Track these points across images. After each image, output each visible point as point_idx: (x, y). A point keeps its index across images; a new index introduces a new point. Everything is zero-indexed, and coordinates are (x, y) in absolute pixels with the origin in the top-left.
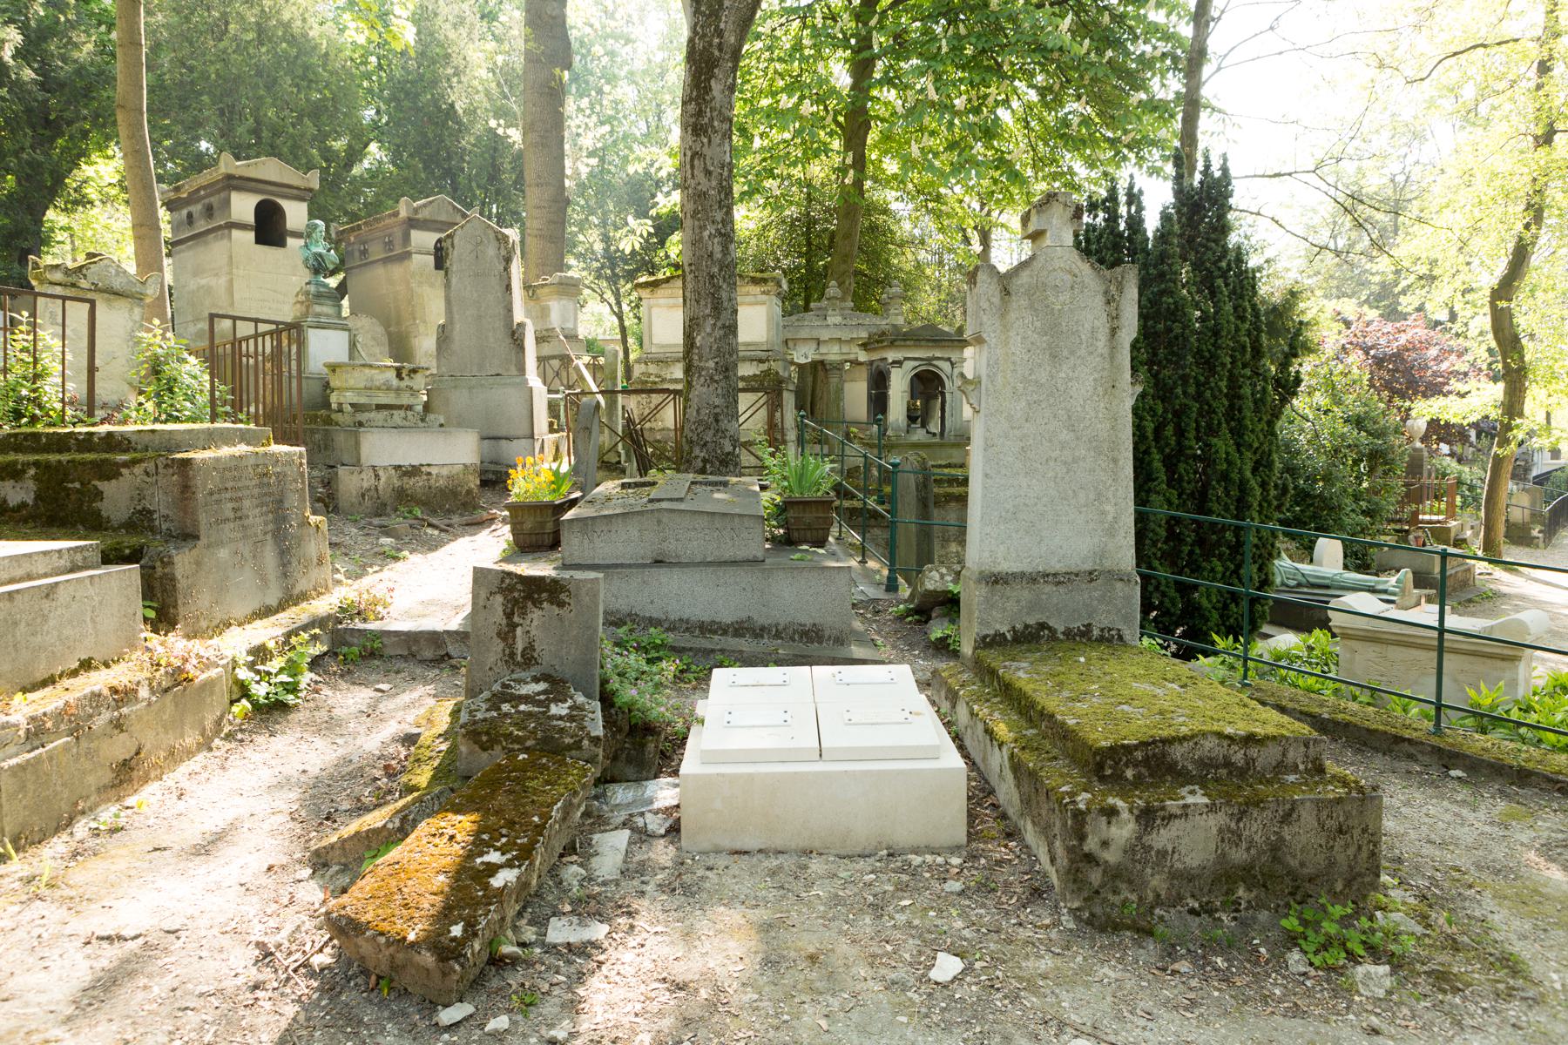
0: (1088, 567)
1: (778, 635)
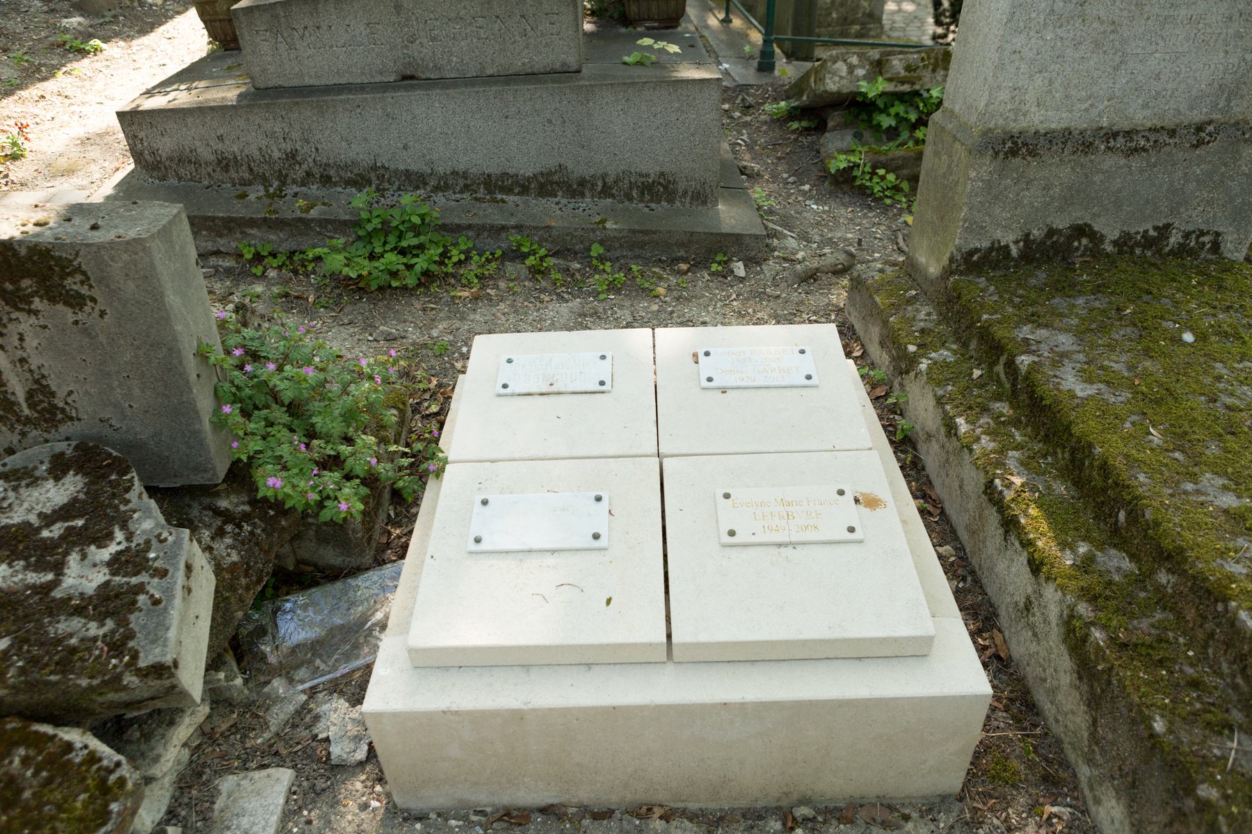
0: (1197, 116)
1: (606, 192)
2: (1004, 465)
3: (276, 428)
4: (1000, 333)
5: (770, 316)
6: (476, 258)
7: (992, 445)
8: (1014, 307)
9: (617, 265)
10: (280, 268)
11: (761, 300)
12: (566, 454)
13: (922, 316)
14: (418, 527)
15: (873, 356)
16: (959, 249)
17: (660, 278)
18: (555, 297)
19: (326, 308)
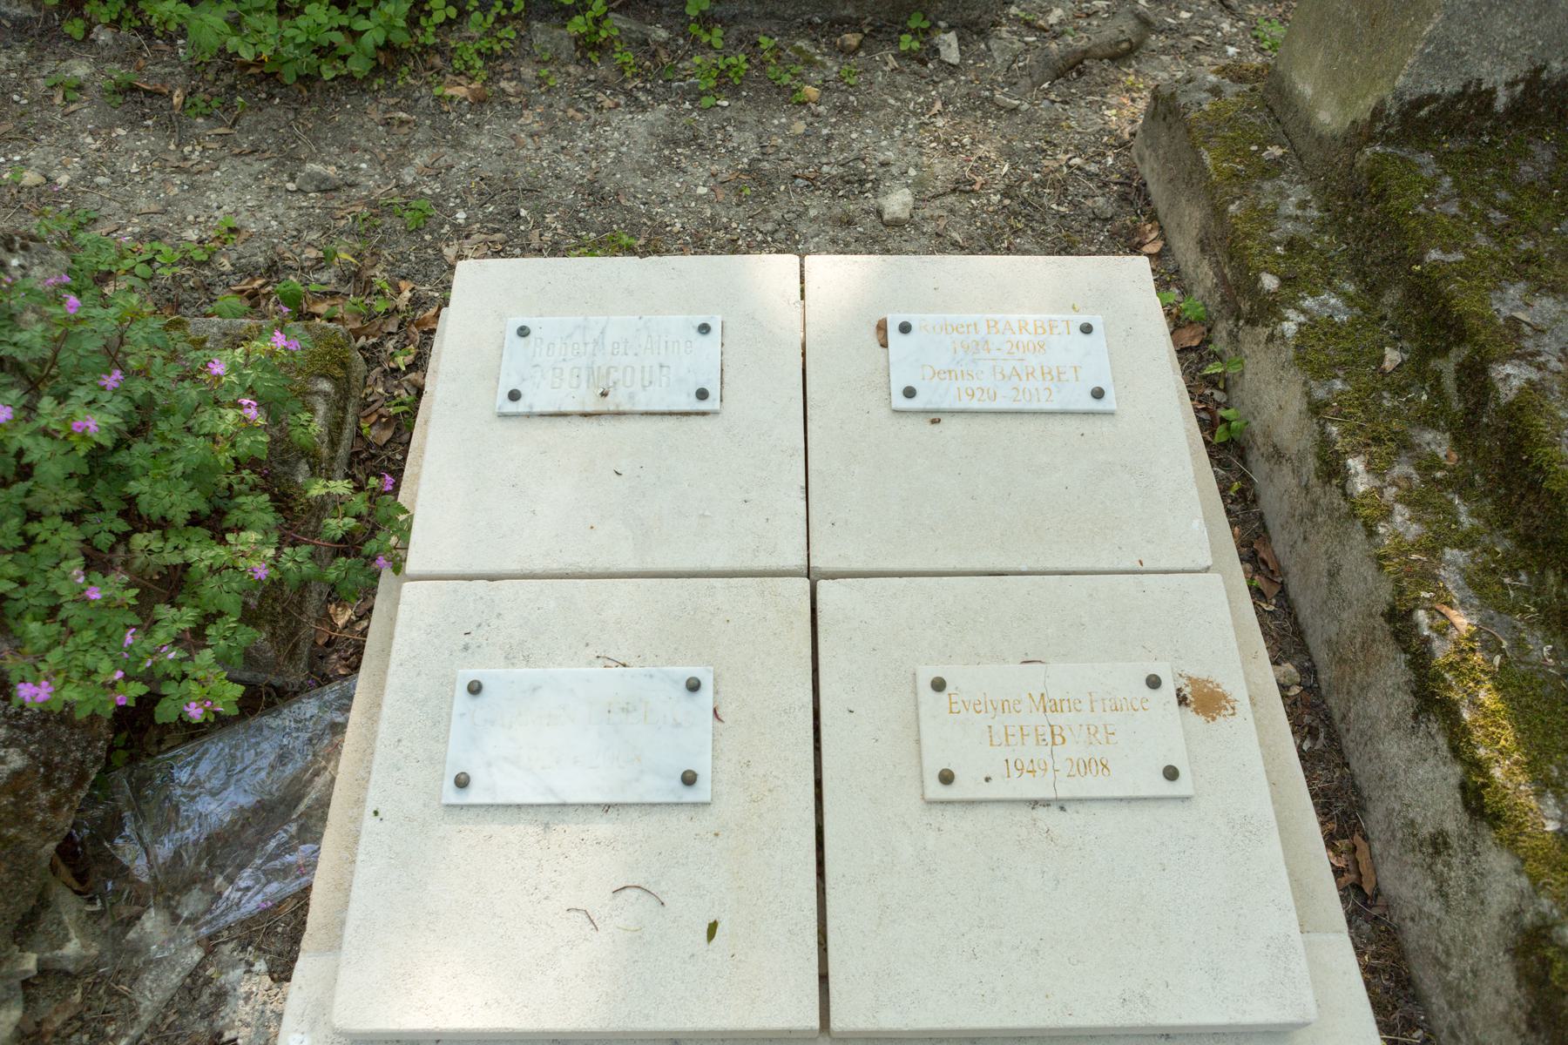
2: (1436, 578)
3: (49, 523)
4: (1465, 303)
5: (1000, 151)
6: (477, 16)
7: (1415, 528)
8: (1488, 234)
9: (734, 32)
10: (116, 24)
11: (985, 116)
12: (633, 566)
13: (1290, 207)
14: (355, 716)
15: (1179, 257)
16: (1398, 96)
17: (810, 63)
18: (622, 100)
19: (208, 117)
